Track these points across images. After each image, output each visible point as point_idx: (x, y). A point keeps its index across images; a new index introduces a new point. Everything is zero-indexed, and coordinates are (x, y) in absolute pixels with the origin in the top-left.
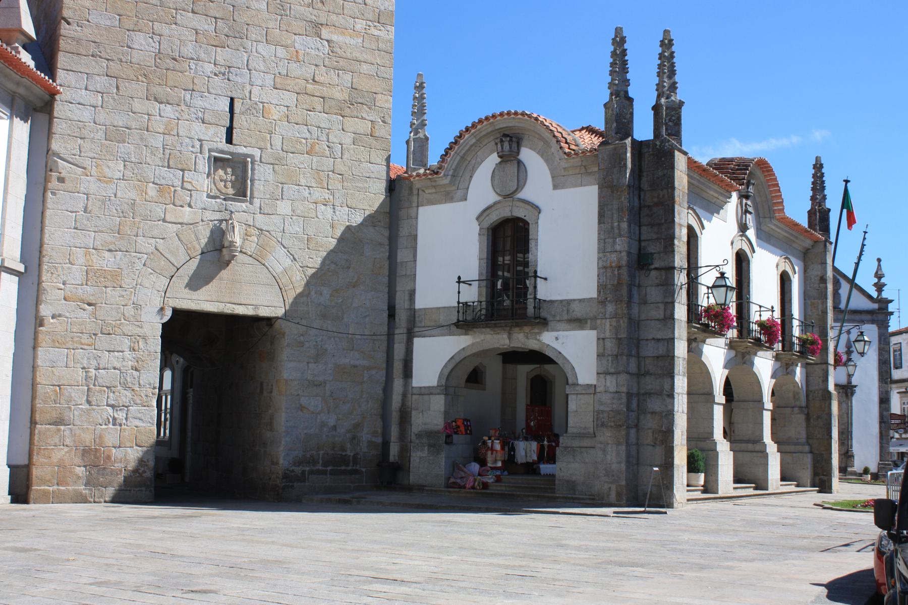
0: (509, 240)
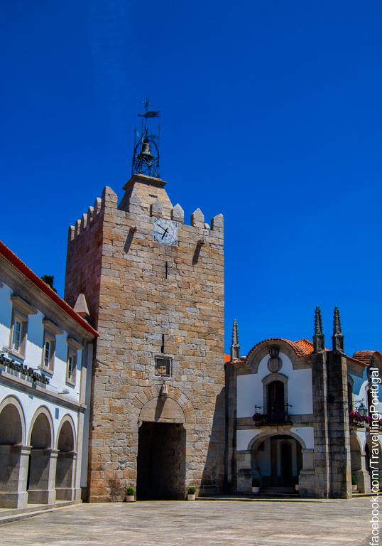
0: (276, 391)
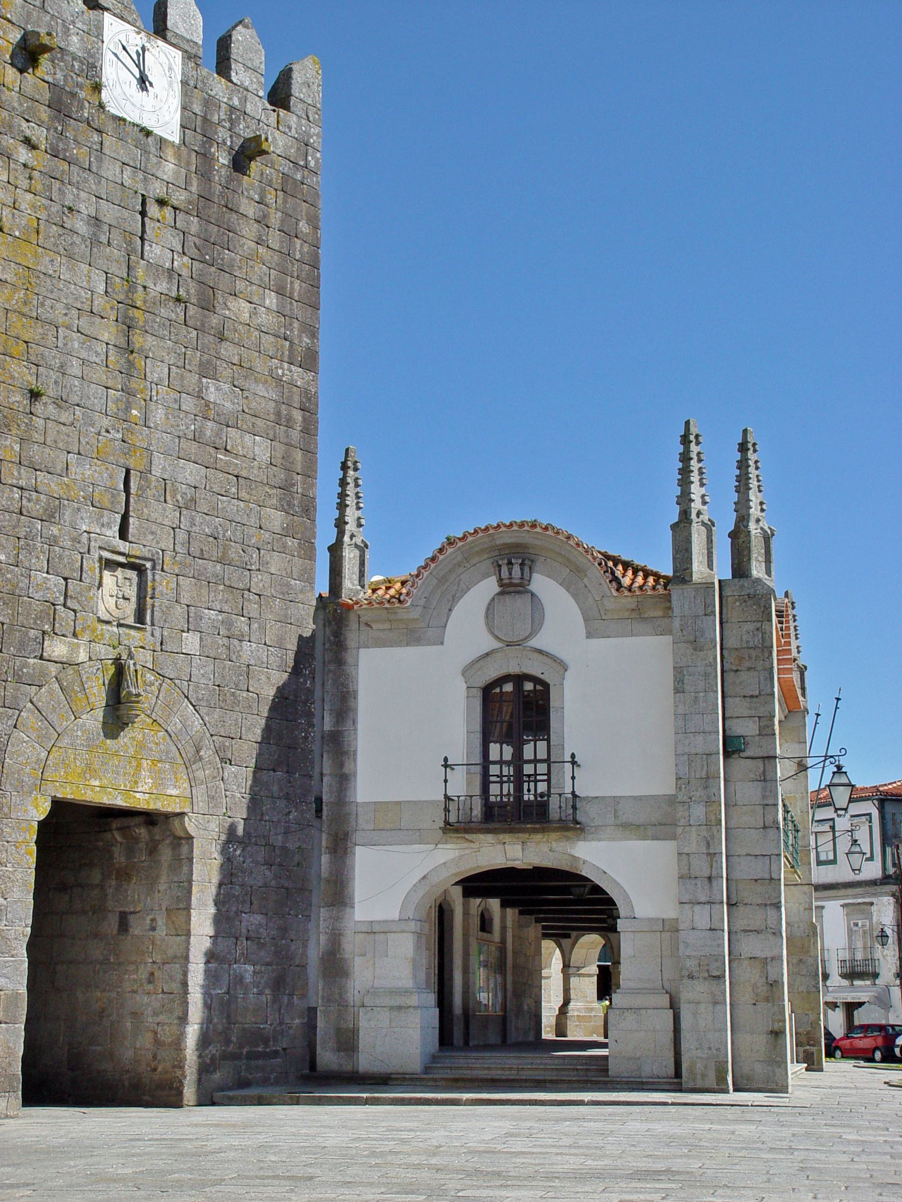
0: (517, 709)
